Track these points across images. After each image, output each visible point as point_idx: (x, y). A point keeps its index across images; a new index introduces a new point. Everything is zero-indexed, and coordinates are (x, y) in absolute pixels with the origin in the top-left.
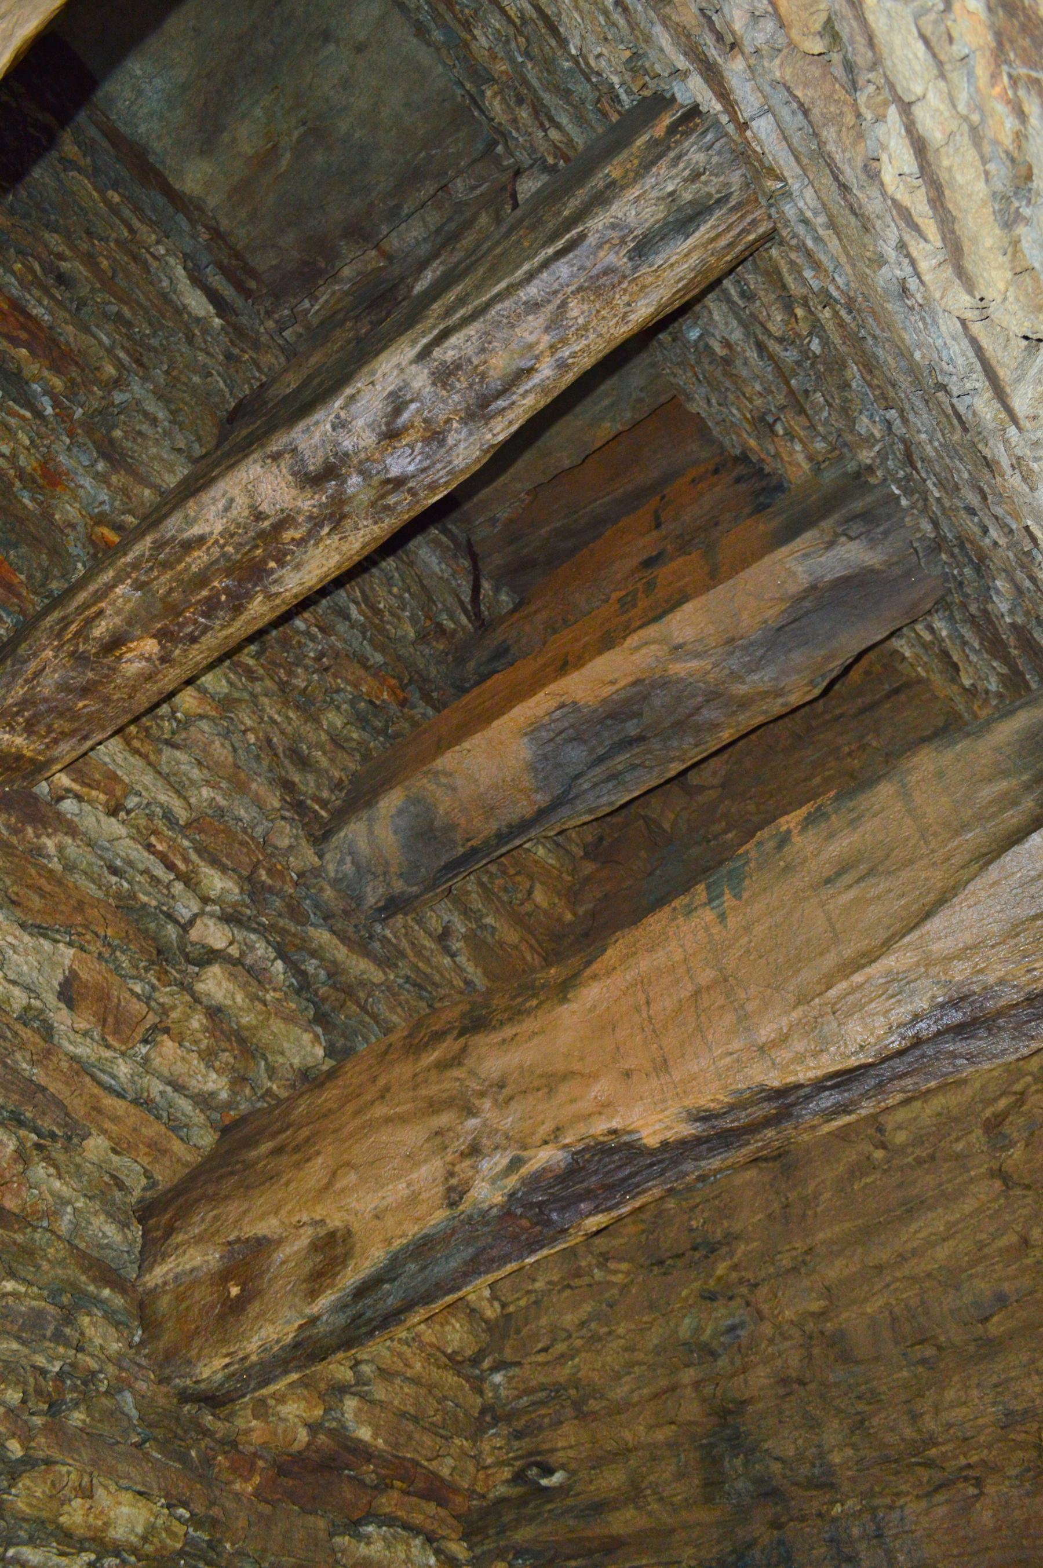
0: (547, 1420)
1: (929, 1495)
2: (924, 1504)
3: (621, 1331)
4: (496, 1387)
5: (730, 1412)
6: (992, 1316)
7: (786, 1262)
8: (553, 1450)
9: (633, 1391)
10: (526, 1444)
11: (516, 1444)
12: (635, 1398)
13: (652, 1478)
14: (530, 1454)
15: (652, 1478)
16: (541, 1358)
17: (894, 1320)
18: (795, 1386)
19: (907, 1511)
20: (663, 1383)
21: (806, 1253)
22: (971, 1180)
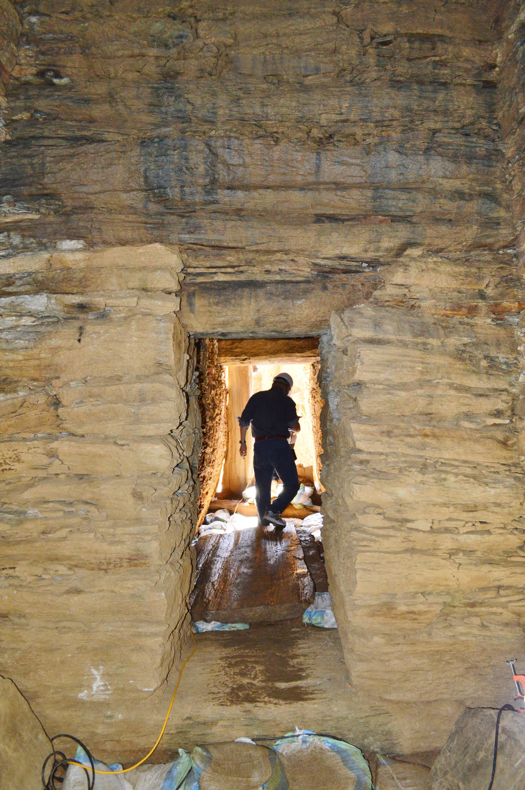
0: (62, 50)
1: (254, 139)
2: (251, 141)
3: (117, 17)
4: (32, 24)
5: (171, 77)
6: (310, 75)
7: (220, 15)
8: (64, 67)
9: (118, 50)
10: (48, 59)
11: (41, 57)
12: (120, 53)
13: (122, 94)
14: (50, 65)
15: (122, 94)
16: (63, 16)
17: (265, 61)
18: (206, 74)
19: (244, 142)
20: (137, 51)
21: (231, 14)
22: (324, 12)
